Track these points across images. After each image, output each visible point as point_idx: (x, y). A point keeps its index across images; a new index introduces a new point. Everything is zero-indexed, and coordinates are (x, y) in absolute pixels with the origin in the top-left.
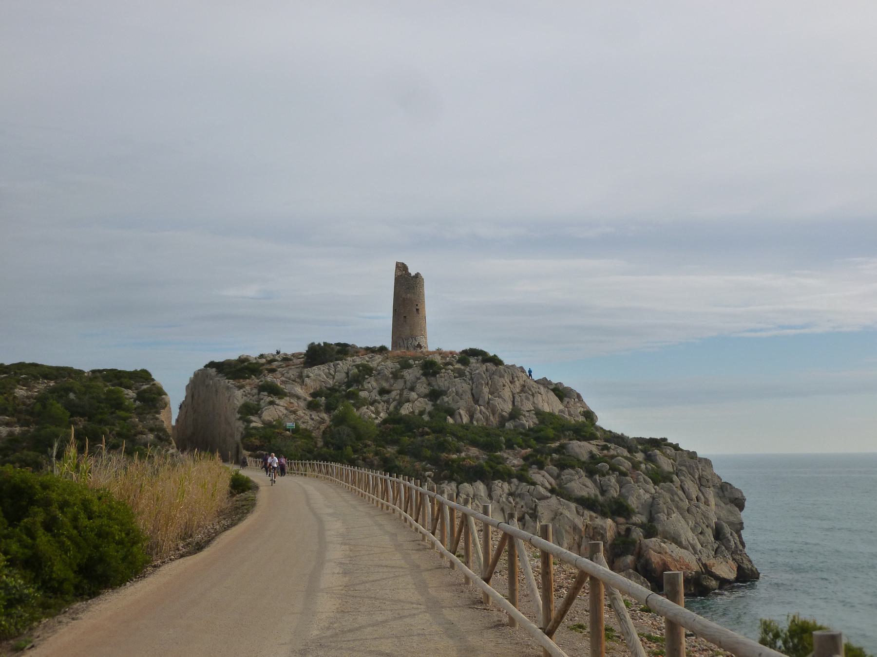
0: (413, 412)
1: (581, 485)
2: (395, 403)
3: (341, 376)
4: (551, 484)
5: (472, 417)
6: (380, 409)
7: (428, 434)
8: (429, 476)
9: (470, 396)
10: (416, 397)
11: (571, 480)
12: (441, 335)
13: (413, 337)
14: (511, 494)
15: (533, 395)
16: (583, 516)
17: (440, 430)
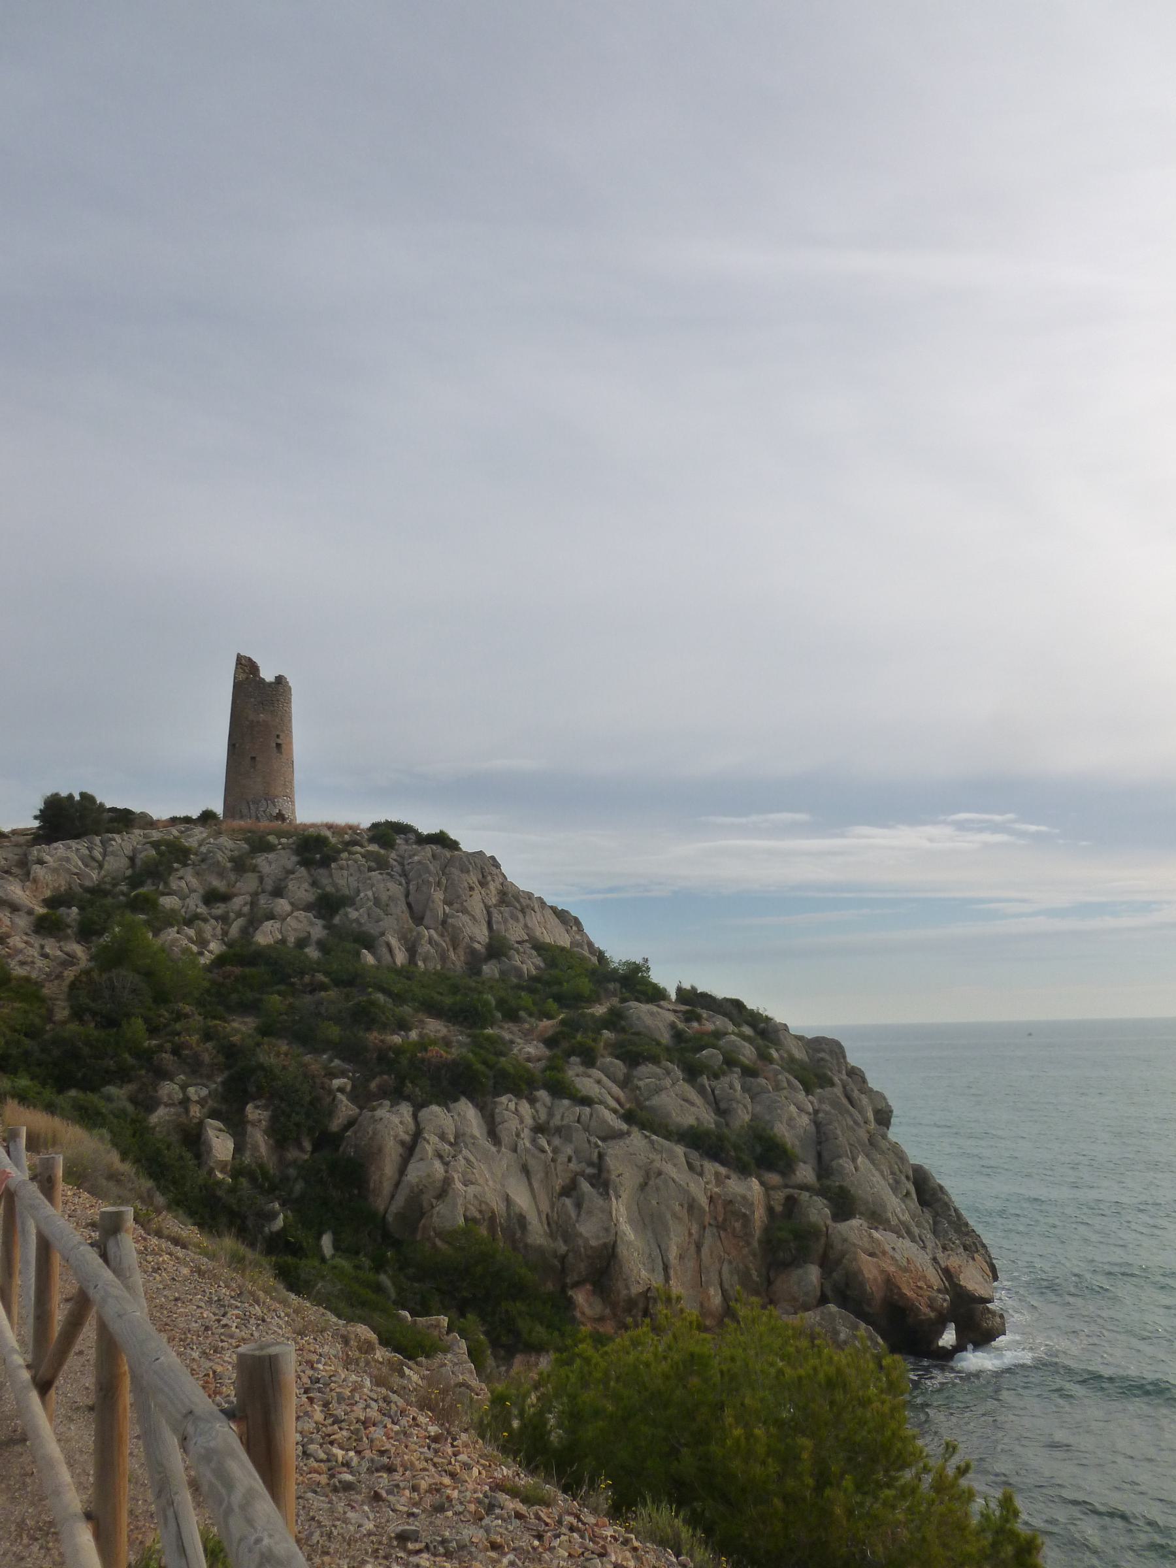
0: (283, 941)
1: (683, 1104)
2: (240, 922)
3: (116, 864)
4: (618, 1101)
5: (412, 951)
6: (208, 935)
7: (323, 987)
8: (341, 1090)
9: (405, 907)
10: (288, 908)
11: (658, 1090)
12: (324, 794)
13: (270, 799)
14: (539, 1129)
15: (523, 911)
16: (701, 1174)
17: (350, 981)
